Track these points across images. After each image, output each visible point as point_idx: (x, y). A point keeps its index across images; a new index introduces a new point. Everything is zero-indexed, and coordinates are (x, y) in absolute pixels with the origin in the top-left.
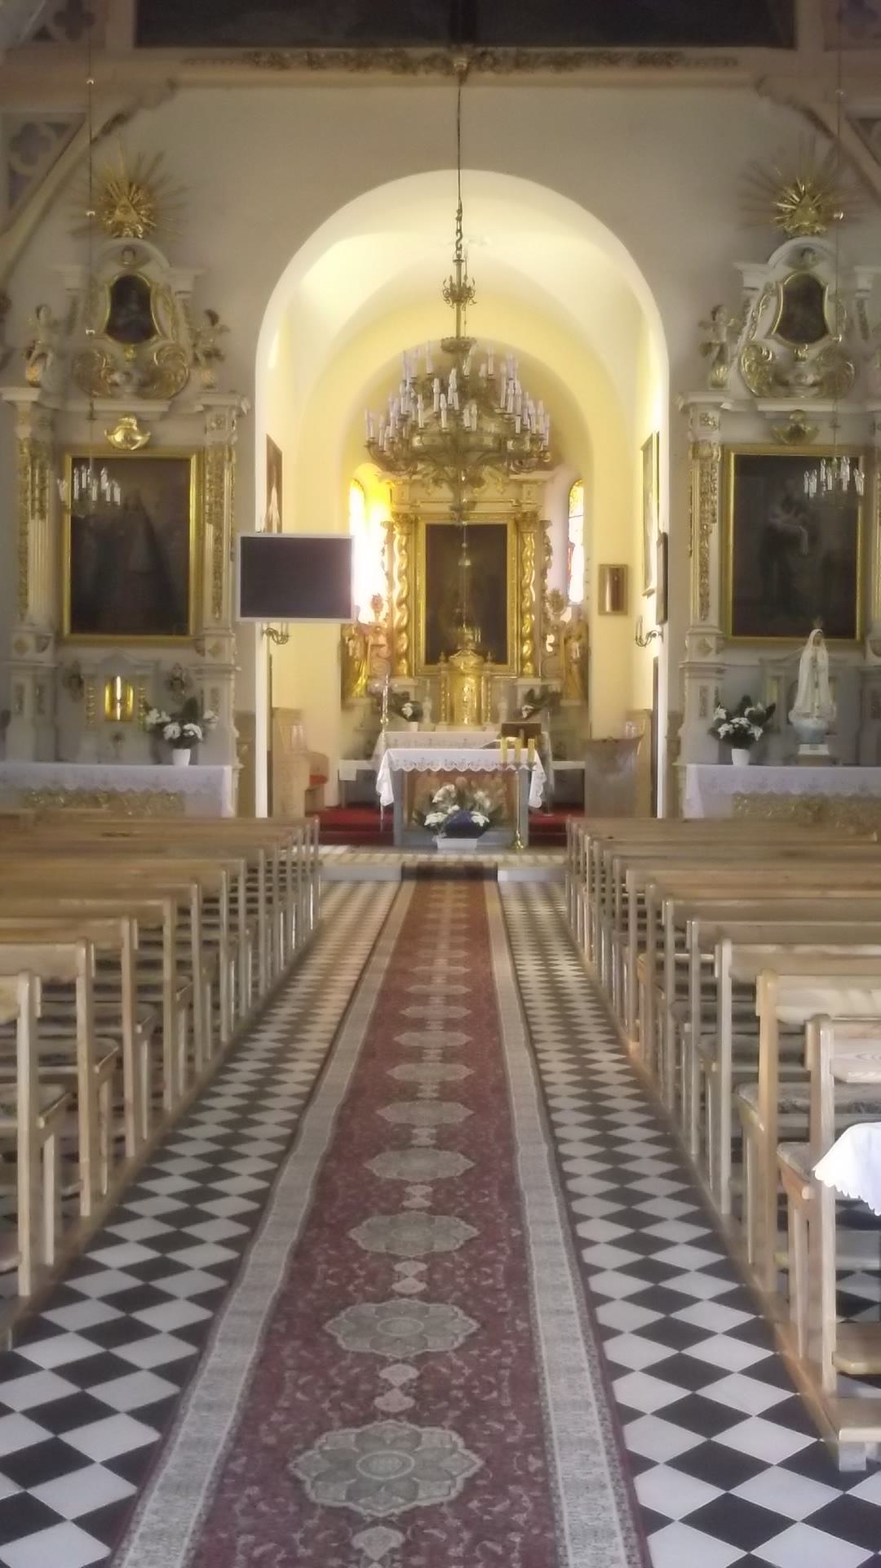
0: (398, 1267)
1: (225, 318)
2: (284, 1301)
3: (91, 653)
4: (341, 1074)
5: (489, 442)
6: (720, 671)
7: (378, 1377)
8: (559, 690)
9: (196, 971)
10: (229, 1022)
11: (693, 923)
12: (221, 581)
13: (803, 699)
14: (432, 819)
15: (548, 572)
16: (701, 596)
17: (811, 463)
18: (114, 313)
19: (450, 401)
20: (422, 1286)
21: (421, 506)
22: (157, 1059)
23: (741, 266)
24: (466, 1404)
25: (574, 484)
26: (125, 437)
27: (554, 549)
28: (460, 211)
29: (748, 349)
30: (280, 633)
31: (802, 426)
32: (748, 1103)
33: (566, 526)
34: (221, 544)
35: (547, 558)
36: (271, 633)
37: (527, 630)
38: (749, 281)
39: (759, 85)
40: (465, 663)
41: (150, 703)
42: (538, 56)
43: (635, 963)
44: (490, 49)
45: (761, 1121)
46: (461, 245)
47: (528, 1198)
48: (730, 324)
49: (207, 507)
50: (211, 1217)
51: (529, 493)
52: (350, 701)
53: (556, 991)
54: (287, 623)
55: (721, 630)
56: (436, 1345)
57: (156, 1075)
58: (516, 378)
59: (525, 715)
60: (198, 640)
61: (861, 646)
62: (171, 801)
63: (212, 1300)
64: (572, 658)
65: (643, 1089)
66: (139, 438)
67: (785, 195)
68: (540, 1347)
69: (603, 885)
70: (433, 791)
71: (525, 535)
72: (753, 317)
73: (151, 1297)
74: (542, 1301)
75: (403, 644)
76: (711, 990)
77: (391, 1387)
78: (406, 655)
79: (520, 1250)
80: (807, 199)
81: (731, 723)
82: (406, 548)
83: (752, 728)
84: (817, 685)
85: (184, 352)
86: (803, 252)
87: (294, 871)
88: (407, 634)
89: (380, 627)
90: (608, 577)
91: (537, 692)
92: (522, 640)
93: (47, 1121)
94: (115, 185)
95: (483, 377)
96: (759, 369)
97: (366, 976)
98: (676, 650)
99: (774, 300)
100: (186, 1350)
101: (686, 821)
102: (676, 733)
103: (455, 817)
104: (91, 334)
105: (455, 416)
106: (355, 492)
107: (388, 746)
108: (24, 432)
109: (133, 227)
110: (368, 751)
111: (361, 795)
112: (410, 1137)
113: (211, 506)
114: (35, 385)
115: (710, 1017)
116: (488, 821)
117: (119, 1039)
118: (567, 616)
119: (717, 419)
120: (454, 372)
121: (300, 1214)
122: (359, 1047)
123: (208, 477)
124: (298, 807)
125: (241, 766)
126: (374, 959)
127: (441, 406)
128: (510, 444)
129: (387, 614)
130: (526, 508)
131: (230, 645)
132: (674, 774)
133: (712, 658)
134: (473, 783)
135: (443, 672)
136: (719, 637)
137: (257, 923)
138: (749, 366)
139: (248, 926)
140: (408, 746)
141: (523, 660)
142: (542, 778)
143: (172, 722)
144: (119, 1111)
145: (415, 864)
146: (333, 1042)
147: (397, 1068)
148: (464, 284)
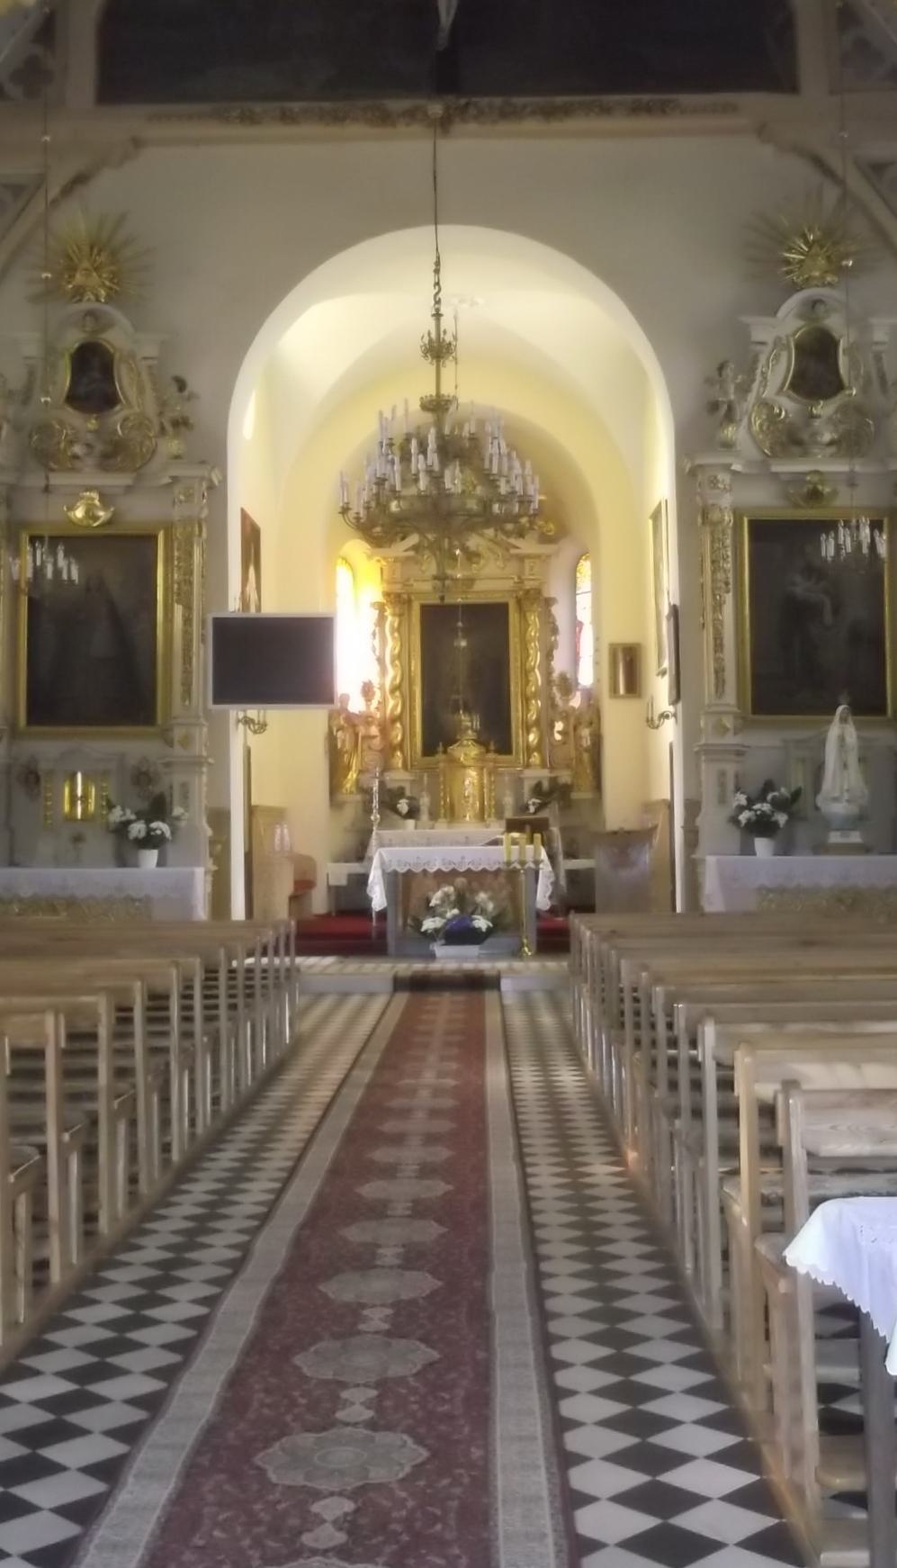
0: (345, 1394)
1: (193, 384)
2: (211, 1433)
3: (47, 747)
4: (303, 1195)
6: (739, 753)
7: (309, 1512)
9: (140, 1078)
11: (680, 1006)
13: (833, 780)
14: (429, 924)
15: (556, 653)
17: (829, 526)
18: (73, 382)
19: (429, 462)
20: (369, 1414)
21: (415, 584)
23: (746, 319)
24: (405, 1538)
25: (580, 558)
26: (87, 512)
27: (560, 628)
28: (438, 263)
29: (759, 407)
30: (256, 722)
31: (820, 487)
32: (731, 1197)
34: (191, 625)
35: (553, 638)
36: (247, 721)
37: (533, 716)
38: (757, 335)
39: (762, 132)
40: (466, 755)
41: (113, 799)
42: (524, 107)
44: (474, 99)
45: (742, 1211)
46: (440, 299)
47: (499, 1319)
48: (738, 381)
49: (176, 586)
51: (532, 569)
52: (341, 797)
53: (553, 1099)
55: (739, 708)
56: (378, 1475)
58: (501, 437)
59: (532, 809)
60: (167, 730)
62: (136, 906)
63: (130, 1434)
64: (581, 746)
66: (101, 513)
67: (793, 245)
68: (495, 1476)
70: (430, 893)
71: (528, 614)
72: (763, 373)
73: (61, 1432)
74: (502, 1426)
75: (397, 734)
77: (323, 1521)
78: (401, 746)
79: (484, 1375)
80: (816, 249)
81: (753, 810)
82: (399, 630)
83: (775, 814)
84: (845, 766)
85: (150, 421)
86: (814, 303)
87: (264, 978)
88: (401, 724)
89: (371, 717)
90: (620, 656)
91: (546, 785)
92: (528, 731)
94: (75, 248)
96: (771, 428)
97: (345, 1091)
98: (690, 733)
99: (784, 355)
100: (95, 1487)
102: (694, 821)
104: (46, 402)
105: (436, 479)
106: (343, 573)
107: (382, 845)
109: (95, 292)
110: (360, 853)
111: (351, 899)
112: (374, 1256)
113: (179, 584)
115: (698, 1113)
116: (491, 925)
117: (43, 1150)
118: (576, 702)
121: (241, 1341)
122: (327, 1165)
123: (176, 554)
125: (214, 868)
126: (355, 1073)
127: (419, 466)
128: (496, 508)
129: (379, 703)
130: (528, 585)
131: (202, 734)
132: (693, 868)
133: (730, 739)
134: (475, 885)
135: (441, 765)
136: (736, 717)
137: (217, 1031)
138: (761, 426)
139: (205, 1033)
140: (404, 845)
141: (529, 750)
142: (549, 878)
143: (138, 819)
144: (41, 1237)
145: (409, 973)
146: (299, 1159)
148: (444, 340)
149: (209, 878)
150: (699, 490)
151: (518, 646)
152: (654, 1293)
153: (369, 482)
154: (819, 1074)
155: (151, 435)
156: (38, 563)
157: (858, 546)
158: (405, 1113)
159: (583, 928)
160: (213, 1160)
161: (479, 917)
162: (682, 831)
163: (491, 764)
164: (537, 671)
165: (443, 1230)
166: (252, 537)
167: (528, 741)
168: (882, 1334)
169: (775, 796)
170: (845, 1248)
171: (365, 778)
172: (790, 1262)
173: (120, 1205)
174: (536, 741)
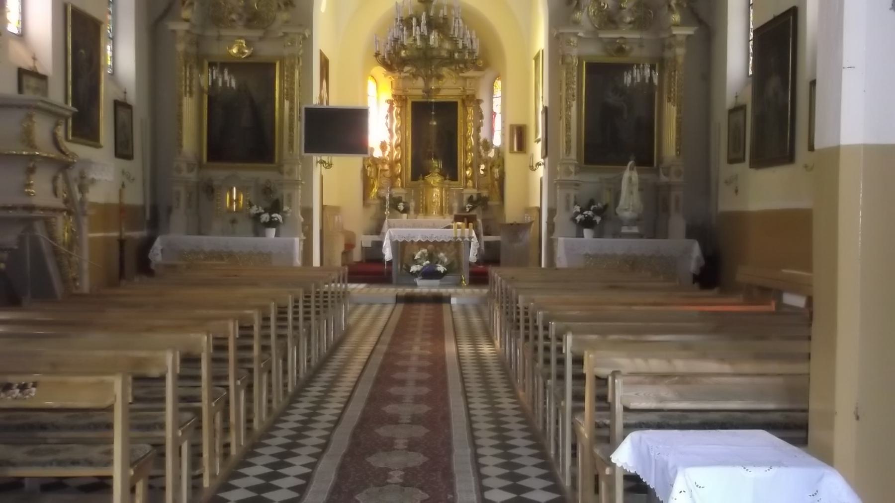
3: (218, 173)
5: (444, 54)
6: (577, 185)
8: (487, 196)
9: (273, 351)
10: (293, 382)
11: (553, 323)
12: (293, 133)
14: (414, 268)
15: (482, 128)
16: (566, 142)
17: (628, 67)
19: (422, 30)
22: (249, 400)
25: (496, 79)
30: (327, 163)
31: (624, 46)
32: (580, 423)
33: (491, 103)
34: (293, 111)
35: (481, 121)
36: (322, 162)
37: (469, 161)
40: (434, 181)
43: (523, 347)
45: (585, 431)
47: (458, 478)
49: (285, 90)
50: (278, 488)
53: (479, 360)
54: (331, 157)
55: (578, 161)
57: (249, 411)
59: (468, 210)
61: (657, 171)
62: (264, 257)
64: (494, 177)
65: (526, 418)
66: (246, 51)
69: (507, 305)
70: (415, 253)
71: (468, 108)
75: (398, 169)
76: (561, 362)
78: (400, 175)
84: (631, 193)
87: (333, 297)
88: (401, 164)
89: (386, 160)
90: (515, 131)
91: (475, 197)
93: (183, 432)
95: (441, 17)
96: (599, 14)
97: (374, 356)
101: (557, 269)
103: (427, 268)
105: (425, 39)
106: (371, 84)
107: (390, 227)
108: (181, 47)
110: (378, 230)
111: (373, 254)
113: (287, 90)
114: (187, 20)
115: (561, 377)
117: (227, 387)
118: (492, 154)
119: (575, 42)
120: (424, 14)
122: (366, 395)
123: (286, 73)
124: (338, 261)
125: (305, 238)
126: (378, 347)
128: (456, 55)
130: (468, 92)
132: (551, 243)
133: (573, 177)
134: (438, 249)
135: (421, 186)
136: (576, 166)
137: (310, 326)
138: (594, 12)
139: (304, 327)
141: (467, 179)
142: (477, 245)
143: (265, 212)
144: (226, 430)
146: (352, 392)
147: (388, 407)
149: (302, 243)
150: (560, 46)
151: (462, 125)
152: (535, 466)
153: (390, 40)
154: (624, 362)
155: (273, 9)
156: (214, 78)
157: (643, 79)
158: (405, 369)
159: (496, 275)
160: (309, 391)
161: (440, 265)
162: (546, 224)
163: (447, 186)
164: (472, 138)
165: (428, 431)
166: (325, 64)
167: (466, 174)
168: (661, 500)
169: (595, 208)
170: (641, 455)
171: (383, 192)
172: (613, 461)
173: (264, 415)
174: (470, 174)
